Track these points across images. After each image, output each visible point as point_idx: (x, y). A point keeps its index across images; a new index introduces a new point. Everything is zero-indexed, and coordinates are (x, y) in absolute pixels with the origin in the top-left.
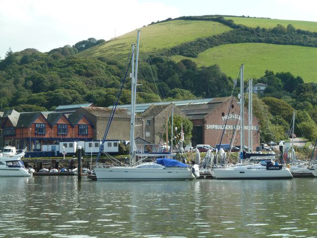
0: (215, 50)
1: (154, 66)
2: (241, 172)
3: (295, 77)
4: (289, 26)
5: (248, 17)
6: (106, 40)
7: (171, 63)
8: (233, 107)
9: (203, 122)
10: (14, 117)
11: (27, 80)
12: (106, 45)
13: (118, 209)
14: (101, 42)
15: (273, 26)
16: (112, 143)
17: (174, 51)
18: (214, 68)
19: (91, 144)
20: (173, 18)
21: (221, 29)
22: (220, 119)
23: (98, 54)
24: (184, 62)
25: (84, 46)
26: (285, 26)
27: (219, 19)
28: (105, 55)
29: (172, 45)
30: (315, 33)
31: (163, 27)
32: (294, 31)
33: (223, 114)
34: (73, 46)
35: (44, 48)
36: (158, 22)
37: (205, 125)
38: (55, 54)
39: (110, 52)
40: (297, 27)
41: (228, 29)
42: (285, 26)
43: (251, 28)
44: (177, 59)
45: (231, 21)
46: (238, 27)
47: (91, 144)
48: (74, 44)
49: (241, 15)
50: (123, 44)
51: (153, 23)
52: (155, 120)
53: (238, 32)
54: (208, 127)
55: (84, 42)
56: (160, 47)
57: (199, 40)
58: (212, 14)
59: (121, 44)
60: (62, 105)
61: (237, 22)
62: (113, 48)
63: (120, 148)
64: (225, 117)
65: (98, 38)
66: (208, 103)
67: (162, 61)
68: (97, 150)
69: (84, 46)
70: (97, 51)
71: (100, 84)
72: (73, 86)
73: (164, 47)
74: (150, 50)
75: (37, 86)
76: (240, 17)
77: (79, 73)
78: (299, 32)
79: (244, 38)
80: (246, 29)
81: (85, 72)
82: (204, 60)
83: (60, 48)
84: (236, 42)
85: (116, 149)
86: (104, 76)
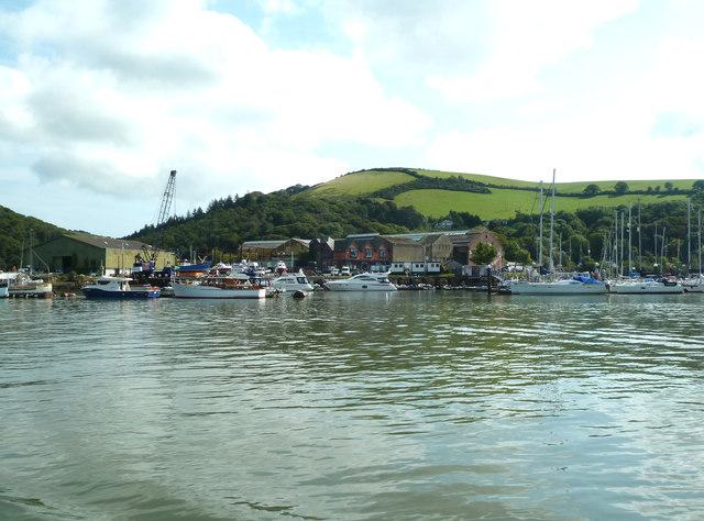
0: (413, 193)
1: (364, 206)
7: (377, 203)
10: (331, 242)
11: (268, 215)
13: (401, 329)
14: (307, 188)
17: (376, 194)
18: (410, 208)
24: (387, 203)
27: (405, 171)
29: (372, 191)
30: (699, 184)
31: (371, 177)
35: (266, 191)
38: (277, 196)
41: (413, 178)
44: (382, 201)
46: (422, 177)
56: (364, 191)
61: (420, 174)
62: (324, 192)
63: (441, 269)
65: (304, 184)
67: (370, 202)
68: (422, 270)
71: (327, 219)
74: (357, 193)
75: (277, 220)
77: (309, 210)
78: (467, 181)
79: (427, 185)
81: (313, 209)
82: (401, 201)
85: (438, 270)
86: (327, 212)
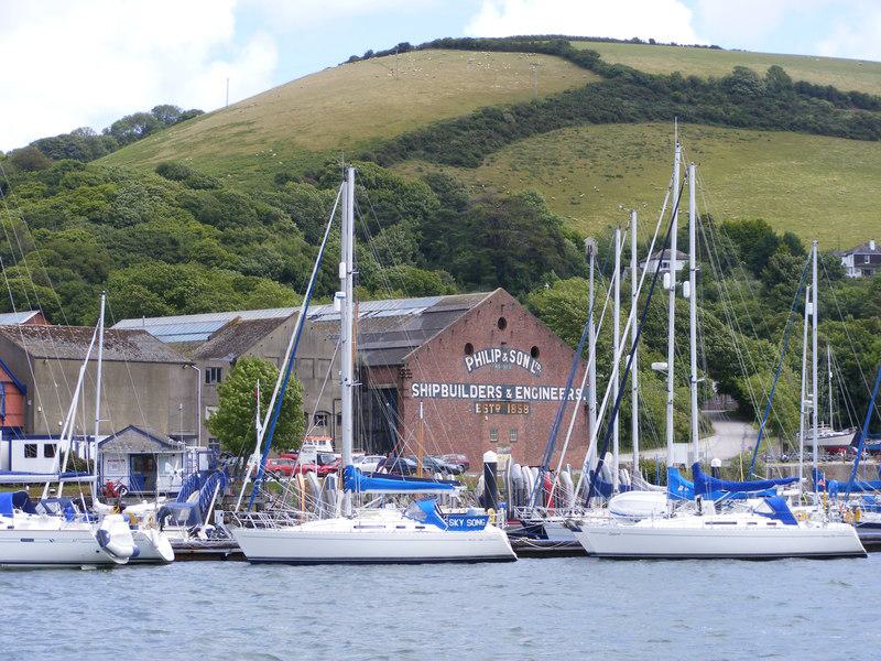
2: (32, 540)
3: (780, 233)
4: (775, 71)
5: (652, 42)
6: (207, 110)
8: (502, 324)
9: (401, 372)
12: (196, 127)
15: (724, 71)
16: (41, 444)
19: (35, 446)
20: (414, 43)
21: (557, 77)
22: (459, 363)
23: (167, 155)
25: (138, 130)
26: (761, 71)
27: (555, 47)
28: (186, 160)
32: (789, 88)
33: (469, 350)
34: (106, 131)
36: (369, 55)
37: (407, 384)
39: (205, 149)
40: (795, 75)
41: (580, 78)
42: (761, 71)
43: (652, 77)
45: (593, 53)
46: (613, 73)
47: (35, 446)
48: (108, 125)
49: (630, 38)
50: (249, 124)
51: (353, 59)
52: (378, 364)
53: (618, 93)
54: (417, 390)
55: (137, 119)
57: (486, 112)
58: (522, 34)
59: (243, 123)
60: (130, 317)
61: (609, 59)
64: (479, 359)
65: (185, 106)
66: (424, 313)
69: (138, 130)
70: (164, 145)
72: (66, 257)
73: (374, 135)
76: (626, 42)
79: (630, 106)
80: (638, 79)
83: (61, 137)
84: (605, 120)
